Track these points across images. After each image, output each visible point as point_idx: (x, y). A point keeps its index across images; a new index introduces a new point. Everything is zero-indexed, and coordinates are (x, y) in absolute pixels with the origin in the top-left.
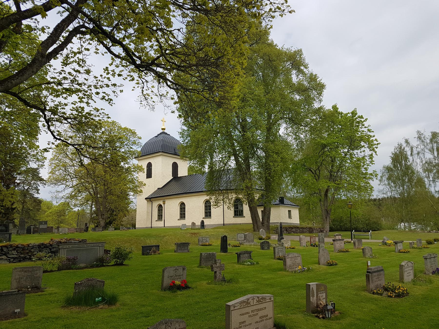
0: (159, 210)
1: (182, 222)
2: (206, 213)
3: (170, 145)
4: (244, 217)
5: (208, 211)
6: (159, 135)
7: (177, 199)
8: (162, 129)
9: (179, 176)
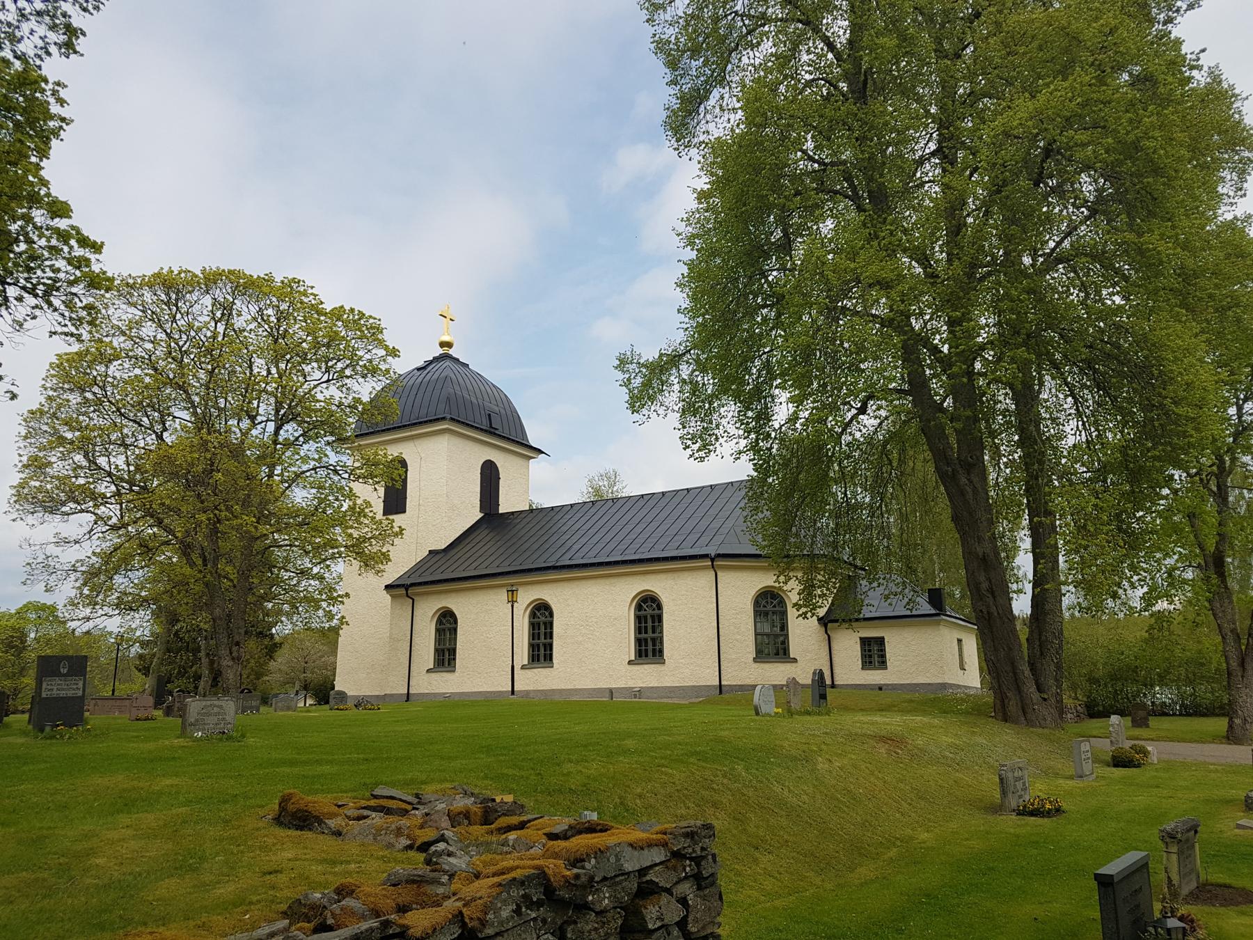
0: (439, 631)
1: (647, 676)
2: (639, 642)
3: (474, 400)
4: (795, 660)
6: (431, 362)
8: (442, 344)
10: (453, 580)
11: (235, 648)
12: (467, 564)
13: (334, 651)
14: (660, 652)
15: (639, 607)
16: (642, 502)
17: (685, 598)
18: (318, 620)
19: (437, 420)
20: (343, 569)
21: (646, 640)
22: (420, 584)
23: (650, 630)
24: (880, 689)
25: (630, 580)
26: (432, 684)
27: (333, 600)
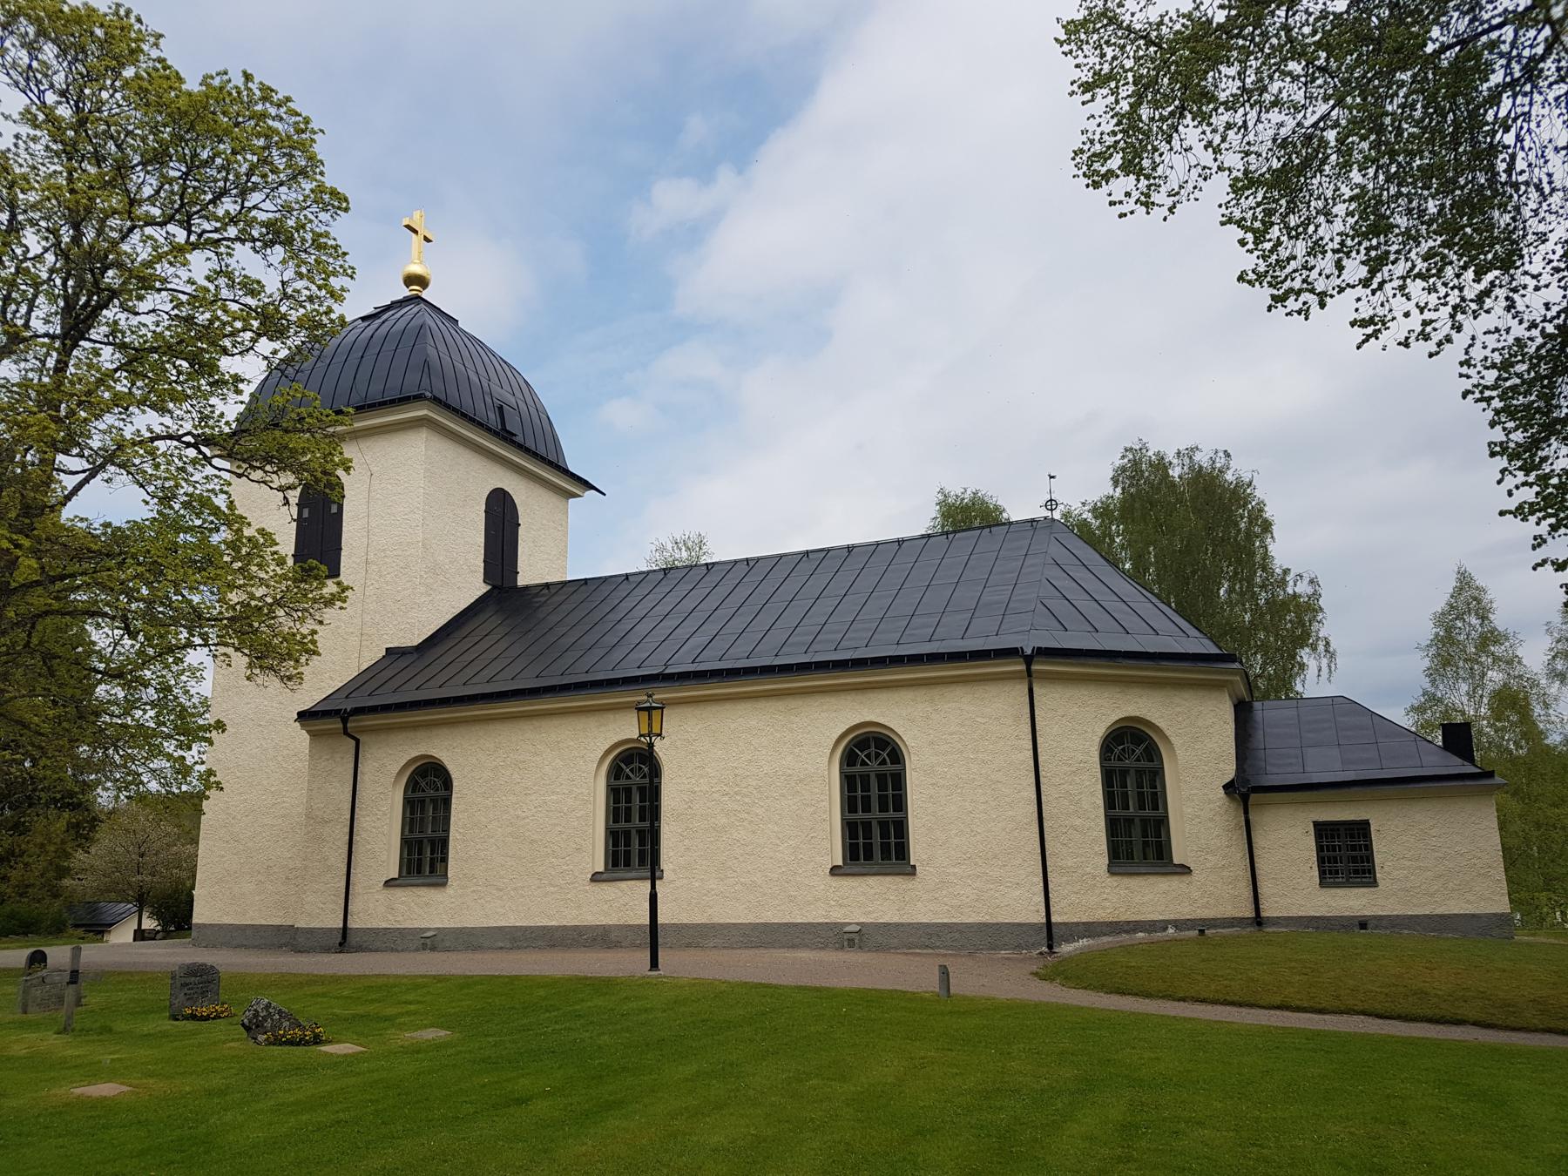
0: (411, 804)
1: (873, 900)
2: (851, 829)
4: (1185, 870)
6: (388, 308)
7: (590, 724)
8: (410, 280)
9: (522, 581)
10: (386, 708)
14: (902, 852)
15: (849, 758)
16: (807, 567)
17: (960, 749)
20: (209, 674)
21: (867, 825)
22: (373, 710)
23: (875, 804)
25: (831, 702)
26: (385, 907)
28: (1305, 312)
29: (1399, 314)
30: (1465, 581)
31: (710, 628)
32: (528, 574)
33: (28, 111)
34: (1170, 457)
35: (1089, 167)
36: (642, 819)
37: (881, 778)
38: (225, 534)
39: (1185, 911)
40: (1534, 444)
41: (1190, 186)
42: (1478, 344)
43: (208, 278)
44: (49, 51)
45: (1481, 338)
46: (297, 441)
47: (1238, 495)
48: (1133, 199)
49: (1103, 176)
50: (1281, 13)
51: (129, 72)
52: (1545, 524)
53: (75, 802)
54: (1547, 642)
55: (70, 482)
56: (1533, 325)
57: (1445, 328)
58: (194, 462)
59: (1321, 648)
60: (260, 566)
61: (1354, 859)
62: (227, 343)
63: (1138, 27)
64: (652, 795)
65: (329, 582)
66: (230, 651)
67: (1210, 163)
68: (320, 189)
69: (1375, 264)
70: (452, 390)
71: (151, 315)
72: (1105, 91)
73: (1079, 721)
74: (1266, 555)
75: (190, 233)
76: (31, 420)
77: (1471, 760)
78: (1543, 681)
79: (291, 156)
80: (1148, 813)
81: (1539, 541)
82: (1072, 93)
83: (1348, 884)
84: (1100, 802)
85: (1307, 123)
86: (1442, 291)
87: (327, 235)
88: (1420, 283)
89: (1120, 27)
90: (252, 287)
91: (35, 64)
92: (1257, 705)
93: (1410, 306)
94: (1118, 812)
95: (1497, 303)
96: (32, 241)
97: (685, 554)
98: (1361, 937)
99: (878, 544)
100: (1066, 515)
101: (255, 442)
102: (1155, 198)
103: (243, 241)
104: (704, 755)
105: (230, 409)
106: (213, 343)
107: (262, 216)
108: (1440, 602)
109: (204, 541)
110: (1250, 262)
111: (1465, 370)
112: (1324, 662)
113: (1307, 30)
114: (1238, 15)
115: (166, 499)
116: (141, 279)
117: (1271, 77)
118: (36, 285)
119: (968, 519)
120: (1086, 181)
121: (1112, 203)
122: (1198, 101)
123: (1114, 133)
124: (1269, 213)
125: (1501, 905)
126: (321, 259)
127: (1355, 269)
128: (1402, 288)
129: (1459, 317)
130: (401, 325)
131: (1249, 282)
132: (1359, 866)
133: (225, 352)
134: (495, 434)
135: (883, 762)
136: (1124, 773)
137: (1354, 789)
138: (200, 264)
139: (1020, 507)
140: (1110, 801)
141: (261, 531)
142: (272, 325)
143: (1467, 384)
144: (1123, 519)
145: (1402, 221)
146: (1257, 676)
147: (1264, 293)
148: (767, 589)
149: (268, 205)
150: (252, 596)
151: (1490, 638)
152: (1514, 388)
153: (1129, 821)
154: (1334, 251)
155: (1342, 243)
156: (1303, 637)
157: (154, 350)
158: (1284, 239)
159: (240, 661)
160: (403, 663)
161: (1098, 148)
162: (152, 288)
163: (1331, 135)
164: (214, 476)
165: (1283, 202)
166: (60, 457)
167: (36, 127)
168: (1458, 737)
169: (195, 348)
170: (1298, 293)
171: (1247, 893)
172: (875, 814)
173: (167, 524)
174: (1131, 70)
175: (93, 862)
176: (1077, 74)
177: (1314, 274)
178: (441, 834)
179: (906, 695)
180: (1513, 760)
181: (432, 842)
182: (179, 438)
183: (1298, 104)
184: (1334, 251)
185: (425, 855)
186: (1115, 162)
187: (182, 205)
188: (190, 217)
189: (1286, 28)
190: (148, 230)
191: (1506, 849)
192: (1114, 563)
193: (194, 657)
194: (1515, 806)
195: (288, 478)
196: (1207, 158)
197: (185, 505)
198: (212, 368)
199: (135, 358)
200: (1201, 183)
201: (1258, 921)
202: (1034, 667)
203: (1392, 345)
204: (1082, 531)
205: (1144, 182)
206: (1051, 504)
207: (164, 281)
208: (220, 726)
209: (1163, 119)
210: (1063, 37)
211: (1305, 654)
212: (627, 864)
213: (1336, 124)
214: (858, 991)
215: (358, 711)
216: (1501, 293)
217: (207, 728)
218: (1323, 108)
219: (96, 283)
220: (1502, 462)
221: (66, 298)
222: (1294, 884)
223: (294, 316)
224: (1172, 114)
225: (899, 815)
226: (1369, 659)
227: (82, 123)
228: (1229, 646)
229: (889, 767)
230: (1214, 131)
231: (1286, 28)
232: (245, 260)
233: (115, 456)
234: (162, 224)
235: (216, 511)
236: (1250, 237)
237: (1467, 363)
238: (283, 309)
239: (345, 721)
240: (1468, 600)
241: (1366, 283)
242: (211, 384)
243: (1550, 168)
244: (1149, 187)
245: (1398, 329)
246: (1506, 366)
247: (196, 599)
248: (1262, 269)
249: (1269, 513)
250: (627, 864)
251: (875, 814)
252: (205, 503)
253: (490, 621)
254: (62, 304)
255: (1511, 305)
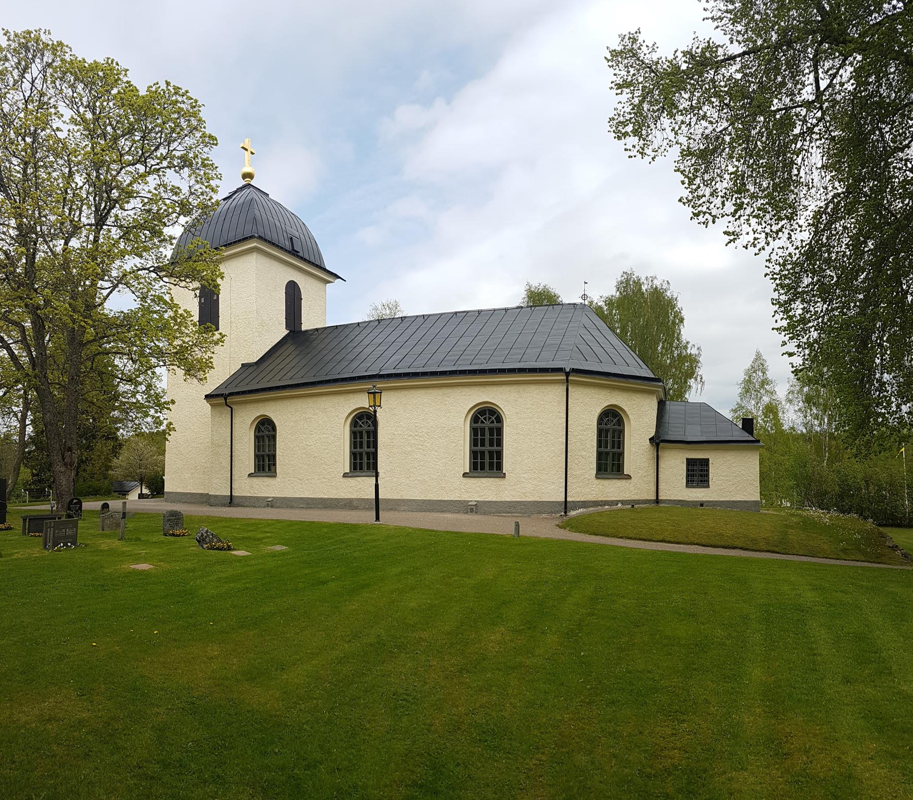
0: (258, 439)
1: (484, 489)
2: (474, 454)
4: (629, 477)
5: (487, 448)
6: (235, 192)
7: (341, 399)
9: (304, 328)
11: (68, 454)
12: (273, 374)
13: (163, 452)
14: (499, 467)
15: (475, 419)
18: (147, 425)
19: (245, 239)
20: (166, 379)
21: (483, 453)
22: (238, 393)
23: (487, 443)
24: (702, 505)
27: (161, 406)
28: (706, 223)
29: (744, 233)
30: (758, 357)
31: (404, 351)
32: (307, 324)
33: (72, 118)
34: (643, 280)
35: (617, 128)
36: (368, 447)
37: (491, 430)
38: (170, 313)
39: (627, 496)
40: (790, 301)
41: (663, 148)
42: (775, 253)
43: (155, 189)
44: (80, 87)
45: (776, 250)
46: (199, 266)
47: (670, 304)
48: (636, 150)
49: (623, 134)
50: (712, 72)
51: (115, 91)
52: (788, 336)
53: (111, 436)
54: (787, 386)
55: (105, 292)
56: (797, 248)
57: (763, 243)
58: (155, 280)
59: (699, 379)
60: (186, 327)
61: (701, 476)
62: (165, 220)
63: (647, 61)
64: (373, 434)
65: (216, 333)
66: (175, 367)
67: (673, 139)
68: (204, 136)
69: (739, 207)
70: (268, 232)
71: (131, 211)
72: (628, 90)
73: (589, 404)
74: (679, 334)
75: (146, 167)
76: (89, 266)
77: (751, 433)
78: (784, 403)
79: (189, 120)
80: (616, 450)
81: (784, 343)
82: (611, 88)
83: (698, 487)
84: (595, 444)
85: (718, 130)
86: (764, 225)
87: (207, 159)
88: (755, 220)
89: (638, 59)
90: (176, 191)
91: (75, 95)
92: (668, 402)
93: (750, 230)
94: (603, 449)
95: (784, 236)
96: (79, 180)
97: (388, 312)
98: (700, 510)
99: (495, 310)
100: (591, 303)
101: (178, 268)
102: (646, 151)
103: (170, 168)
104: (398, 415)
105: (168, 252)
106: (160, 221)
107: (178, 154)
108: (748, 365)
109: (161, 317)
110: (686, 193)
111: (767, 264)
112: (700, 386)
113: (722, 84)
114: (692, 68)
115: (144, 298)
116: (127, 193)
117: (704, 104)
118: (82, 201)
119: (541, 300)
120: (614, 135)
121: (626, 150)
122: (670, 107)
123: (630, 113)
124: (696, 170)
125: (756, 497)
126: (203, 170)
127: (730, 207)
128: (748, 220)
129: (769, 239)
130: (241, 201)
131: (684, 203)
132: (703, 479)
133: (165, 225)
134: (289, 252)
135: (493, 422)
136: (607, 431)
137: (705, 445)
138: (153, 180)
139: (567, 298)
140: (599, 444)
141: (185, 311)
142: (185, 208)
143: (768, 271)
144: (618, 308)
145: (751, 188)
146: (670, 389)
147: (688, 211)
148: (434, 331)
149: (180, 148)
150: (184, 342)
151: (765, 382)
152: (785, 276)
153: (607, 453)
154: (722, 197)
155: (725, 193)
156: (691, 374)
157: (134, 227)
158: (702, 185)
159: (180, 372)
160: (251, 370)
161: (621, 119)
162: (132, 197)
163: (727, 138)
164: (160, 287)
165: (703, 166)
166: (100, 282)
167: (76, 125)
168: (748, 424)
169: (152, 223)
170: (705, 213)
171: (654, 489)
172: (486, 446)
173: (147, 310)
174: (641, 83)
175: (121, 461)
176: (614, 78)
177: (712, 206)
178: (272, 452)
179: (506, 389)
180: (769, 435)
181: (268, 456)
182: (148, 269)
183: (714, 120)
184: (722, 197)
185: (265, 462)
186: (629, 128)
187: (143, 153)
188: (146, 159)
189: (713, 81)
190: (128, 168)
191: (761, 473)
192: (613, 330)
193: (158, 370)
194: (767, 454)
195: (196, 284)
196: (671, 136)
197: (153, 300)
198: (161, 233)
199: (127, 232)
200: (668, 148)
201: (657, 501)
202: (570, 378)
203: (740, 247)
204: (598, 311)
205: (642, 142)
206: (584, 297)
207: (138, 193)
208: (173, 402)
209: (654, 111)
210: (609, 58)
211: (692, 382)
212: (361, 469)
213: (730, 134)
214: (476, 534)
215: (231, 394)
216: (786, 232)
217: (167, 403)
218: (725, 124)
219: (109, 197)
220: (776, 307)
221: (96, 206)
222: (675, 486)
223: (195, 203)
224: (658, 110)
225: (499, 448)
226: (716, 389)
227: (97, 119)
228: (659, 374)
229: (496, 424)
230: (676, 123)
231: (713, 81)
232: (171, 178)
233: (122, 280)
234: (133, 165)
235: (165, 303)
236: (686, 180)
237: (769, 261)
238: (190, 200)
239: (226, 399)
240: (759, 365)
241: (733, 215)
242: (159, 241)
243: (813, 176)
244: (644, 145)
245: (744, 239)
246: (784, 265)
247: (161, 345)
248: (690, 198)
249: (684, 313)
250: (361, 469)
251: (486, 446)
252: (160, 299)
253: (289, 349)
254: (93, 209)
255: (789, 238)
